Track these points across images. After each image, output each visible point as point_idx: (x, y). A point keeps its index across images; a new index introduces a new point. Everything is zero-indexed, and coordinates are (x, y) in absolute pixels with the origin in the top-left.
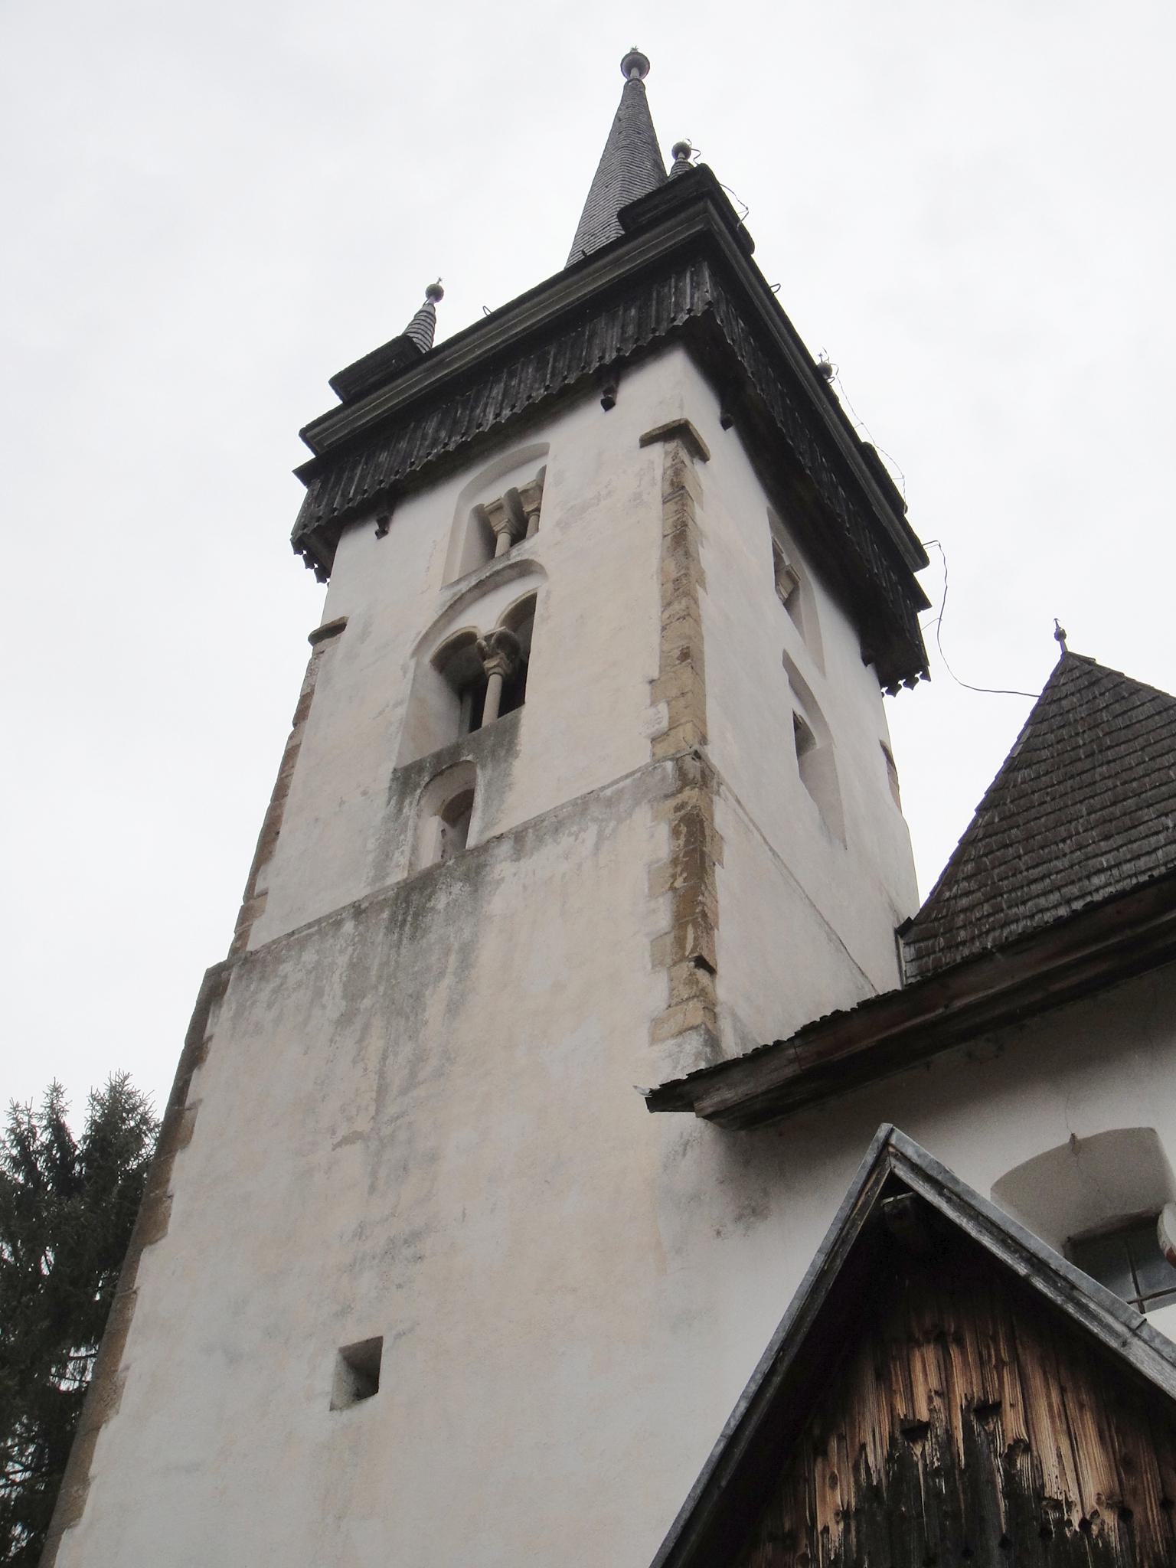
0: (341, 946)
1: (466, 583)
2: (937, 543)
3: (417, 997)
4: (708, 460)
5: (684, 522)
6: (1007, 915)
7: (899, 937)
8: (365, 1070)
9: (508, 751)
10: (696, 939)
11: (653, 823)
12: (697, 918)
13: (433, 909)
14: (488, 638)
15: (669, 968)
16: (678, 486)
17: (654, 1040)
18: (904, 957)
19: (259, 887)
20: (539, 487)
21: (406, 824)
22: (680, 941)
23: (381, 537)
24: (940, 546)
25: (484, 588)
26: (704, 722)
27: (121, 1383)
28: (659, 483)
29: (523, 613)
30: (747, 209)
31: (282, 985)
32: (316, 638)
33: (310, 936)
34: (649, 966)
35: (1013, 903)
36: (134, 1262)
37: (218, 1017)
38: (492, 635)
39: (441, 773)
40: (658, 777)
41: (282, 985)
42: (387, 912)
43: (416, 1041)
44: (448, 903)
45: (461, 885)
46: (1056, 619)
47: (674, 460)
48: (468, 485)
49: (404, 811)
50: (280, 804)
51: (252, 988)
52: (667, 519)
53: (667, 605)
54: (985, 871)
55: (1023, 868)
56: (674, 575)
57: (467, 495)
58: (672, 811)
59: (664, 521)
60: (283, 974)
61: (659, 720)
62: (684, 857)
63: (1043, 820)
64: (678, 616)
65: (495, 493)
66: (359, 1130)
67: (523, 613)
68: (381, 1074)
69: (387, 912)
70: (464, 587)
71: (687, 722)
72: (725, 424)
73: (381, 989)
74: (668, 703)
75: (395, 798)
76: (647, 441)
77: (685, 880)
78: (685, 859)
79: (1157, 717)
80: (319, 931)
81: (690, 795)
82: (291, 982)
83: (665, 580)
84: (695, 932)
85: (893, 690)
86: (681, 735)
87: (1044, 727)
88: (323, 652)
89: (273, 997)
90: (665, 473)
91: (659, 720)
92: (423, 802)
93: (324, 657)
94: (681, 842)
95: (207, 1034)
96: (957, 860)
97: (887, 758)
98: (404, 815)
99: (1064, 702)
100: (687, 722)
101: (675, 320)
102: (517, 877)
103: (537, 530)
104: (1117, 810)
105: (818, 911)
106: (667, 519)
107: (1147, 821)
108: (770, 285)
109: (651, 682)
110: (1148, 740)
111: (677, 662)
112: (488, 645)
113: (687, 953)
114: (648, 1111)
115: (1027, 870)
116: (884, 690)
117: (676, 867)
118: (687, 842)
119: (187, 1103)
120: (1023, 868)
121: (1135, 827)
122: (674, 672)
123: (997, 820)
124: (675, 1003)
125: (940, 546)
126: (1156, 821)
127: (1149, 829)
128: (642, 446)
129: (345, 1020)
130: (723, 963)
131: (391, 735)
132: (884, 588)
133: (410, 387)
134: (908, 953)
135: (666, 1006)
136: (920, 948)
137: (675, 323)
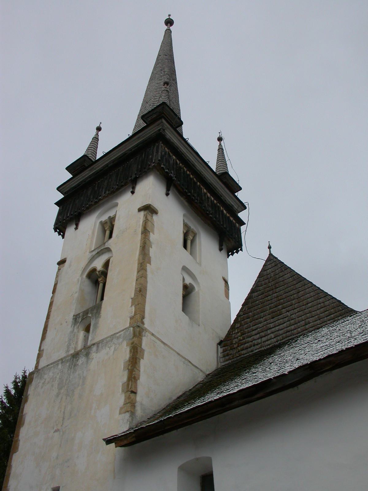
2: (247, 203)
4: (158, 213)
5: (145, 242)
6: (246, 340)
8: (61, 411)
10: (131, 385)
13: (78, 364)
14: (99, 272)
15: (126, 393)
17: (120, 413)
19: (42, 348)
20: (115, 215)
21: (74, 335)
22: (128, 385)
25: (99, 254)
26: (144, 312)
28: (141, 227)
29: (107, 264)
31: (45, 381)
33: (51, 367)
34: (121, 392)
38: (100, 271)
39: (84, 319)
40: (129, 333)
41: (45, 381)
48: (97, 216)
51: (38, 381)
53: (138, 272)
57: (98, 217)
59: (141, 241)
65: (105, 218)
66: (59, 428)
67: (107, 264)
68: (64, 413)
70: (94, 253)
71: (138, 314)
73: (66, 387)
74: (135, 306)
76: (140, 210)
77: (131, 367)
79: (290, 278)
81: (135, 340)
82: (47, 381)
84: (131, 383)
86: (137, 318)
87: (262, 279)
90: (143, 223)
92: (79, 327)
94: (131, 355)
95: (28, 394)
98: (75, 332)
100: (138, 314)
109: (132, 298)
110: (250, 325)
112: (99, 274)
115: (252, 326)
118: (133, 355)
120: (251, 326)
121: (280, 315)
123: (247, 309)
126: (286, 313)
129: (58, 395)
133: (86, 175)
134: (220, 350)
136: (224, 349)
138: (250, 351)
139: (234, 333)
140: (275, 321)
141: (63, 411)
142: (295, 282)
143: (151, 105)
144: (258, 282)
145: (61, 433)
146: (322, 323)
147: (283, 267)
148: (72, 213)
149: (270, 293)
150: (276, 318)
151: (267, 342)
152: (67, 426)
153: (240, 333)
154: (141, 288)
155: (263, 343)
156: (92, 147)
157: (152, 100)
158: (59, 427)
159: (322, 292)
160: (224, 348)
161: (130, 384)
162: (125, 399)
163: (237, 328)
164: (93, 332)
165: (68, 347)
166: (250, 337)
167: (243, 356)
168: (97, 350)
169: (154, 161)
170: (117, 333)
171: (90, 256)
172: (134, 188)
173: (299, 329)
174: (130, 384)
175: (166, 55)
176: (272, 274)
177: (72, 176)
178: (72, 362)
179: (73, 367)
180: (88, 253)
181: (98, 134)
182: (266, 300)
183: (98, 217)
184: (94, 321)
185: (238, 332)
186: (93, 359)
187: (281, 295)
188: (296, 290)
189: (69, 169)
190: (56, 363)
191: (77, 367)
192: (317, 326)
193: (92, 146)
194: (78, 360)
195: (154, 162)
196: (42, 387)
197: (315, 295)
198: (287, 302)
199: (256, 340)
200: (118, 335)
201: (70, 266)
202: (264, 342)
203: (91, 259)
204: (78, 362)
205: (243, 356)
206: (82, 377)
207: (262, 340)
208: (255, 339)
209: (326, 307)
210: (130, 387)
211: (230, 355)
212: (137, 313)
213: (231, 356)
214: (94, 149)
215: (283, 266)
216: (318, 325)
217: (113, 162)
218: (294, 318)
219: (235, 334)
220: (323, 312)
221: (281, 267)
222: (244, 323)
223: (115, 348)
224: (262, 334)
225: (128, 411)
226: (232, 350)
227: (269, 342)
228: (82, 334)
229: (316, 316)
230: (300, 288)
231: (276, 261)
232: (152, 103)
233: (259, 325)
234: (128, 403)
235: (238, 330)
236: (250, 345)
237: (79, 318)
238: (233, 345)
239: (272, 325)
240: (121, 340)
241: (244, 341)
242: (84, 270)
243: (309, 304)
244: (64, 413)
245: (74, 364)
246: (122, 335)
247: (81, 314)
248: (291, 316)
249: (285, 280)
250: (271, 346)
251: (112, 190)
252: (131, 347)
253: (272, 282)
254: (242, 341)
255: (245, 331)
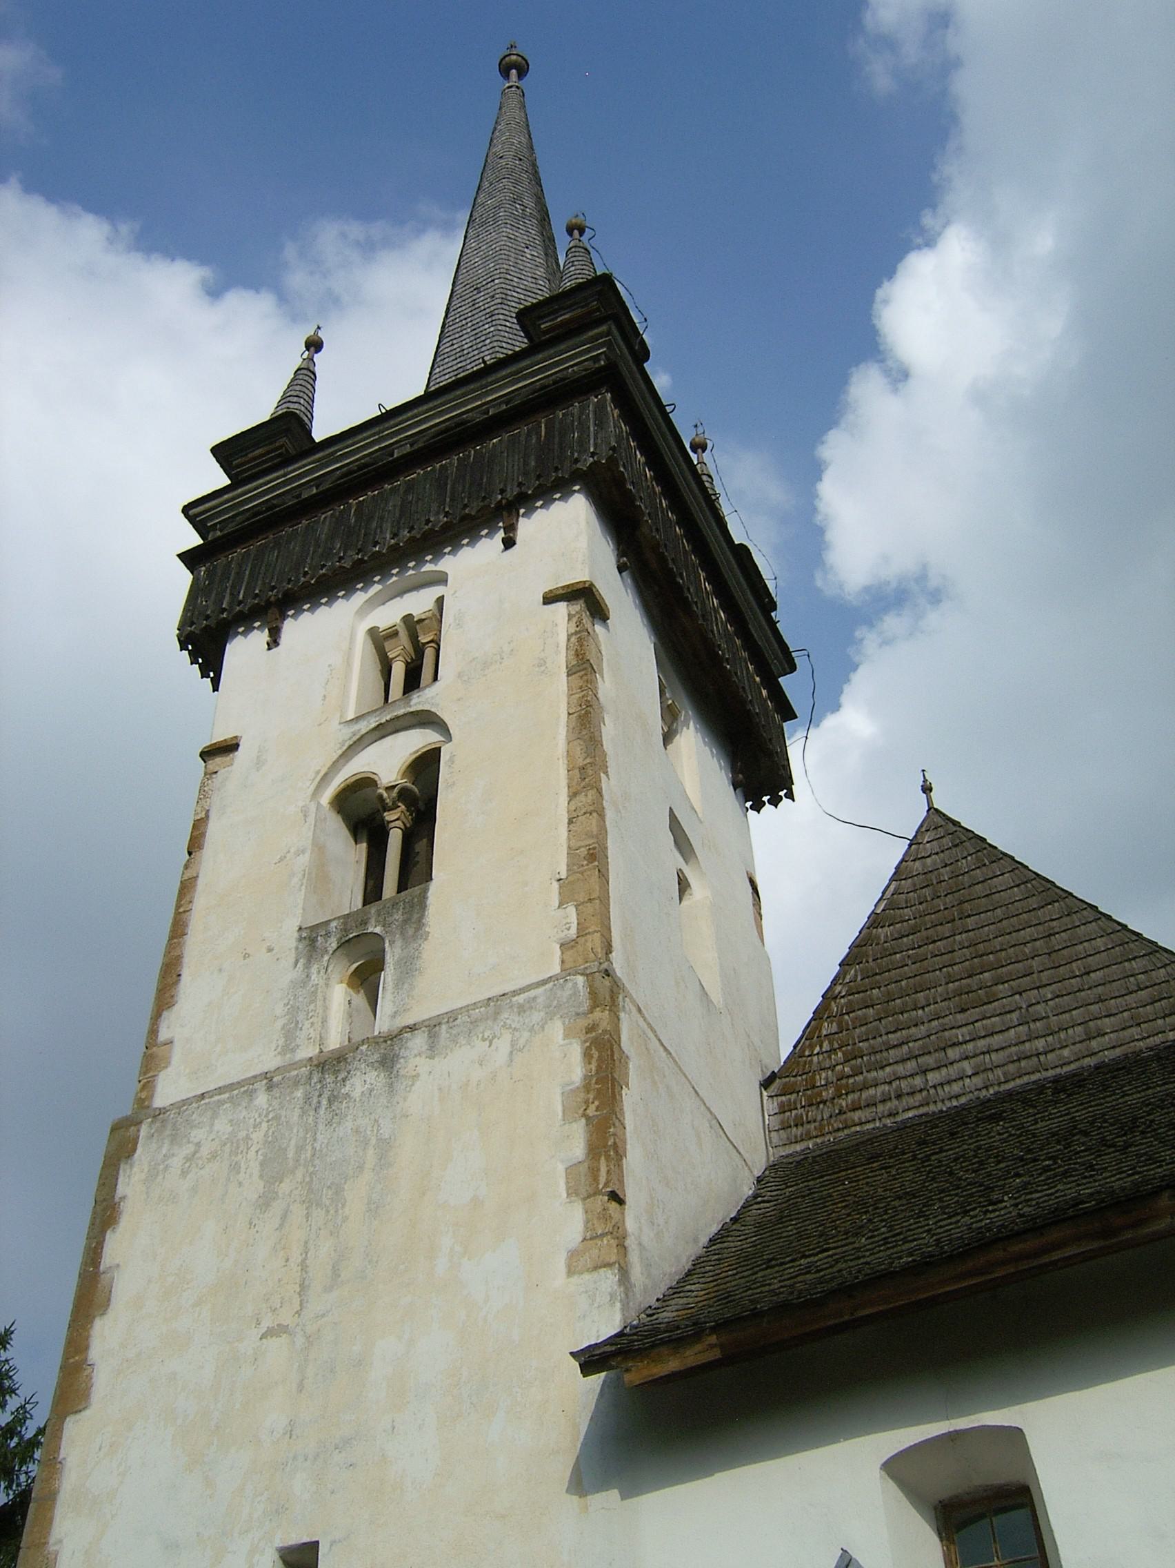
0: (255, 1120)
1: (365, 723)
3: (338, 1190)
6: (865, 1078)
7: (763, 1089)
9: (418, 929)
11: (566, 1041)
12: (609, 1151)
14: (390, 789)
16: (583, 658)
17: (570, 1272)
18: (768, 1110)
21: (314, 993)
22: (594, 1173)
23: (626, 1499)
24: (809, 656)
25: (382, 731)
27: (53, 1557)
30: (646, 320)
31: (195, 1152)
32: (208, 754)
33: (222, 1103)
35: (873, 1068)
36: (57, 1430)
37: (129, 1176)
38: (394, 787)
41: (195, 1152)
42: (301, 1091)
43: (338, 1237)
44: (363, 1092)
45: (376, 1074)
46: (923, 771)
47: (577, 626)
49: (313, 978)
50: (179, 943)
51: (164, 1151)
52: (572, 695)
53: (573, 796)
54: (847, 1030)
55: (883, 1032)
56: (580, 762)
58: (584, 1031)
59: (570, 695)
60: (196, 1140)
61: (568, 926)
62: (596, 1083)
63: (903, 983)
64: (584, 811)
65: (389, 615)
68: (304, 1266)
69: (301, 1091)
70: (365, 726)
71: (595, 931)
72: (621, 569)
74: (577, 907)
75: (301, 960)
76: (549, 599)
78: (597, 1086)
79: (1016, 889)
80: (231, 1099)
81: (602, 1016)
82: (205, 1151)
83: (571, 766)
85: (757, 807)
88: (216, 772)
89: (187, 1165)
91: (568, 926)
93: (218, 779)
94: (593, 1066)
96: (820, 1014)
97: (753, 889)
98: (312, 983)
99: (929, 860)
100: (595, 931)
101: (579, 461)
102: (431, 1077)
103: (435, 679)
104: (973, 982)
105: (702, 1100)
106: (572, 695)
107: (1002, 998)
108: (665, 403)
110: (877, 1029)
111: (585, 862)
113: (601, 1187)
114: (581, 1376)
116: (748, 804)
117: (588, 1093)
118: (599, 1068)
119: (102, 1268)
120: (883, 1032)
121: (990, 1003)
122: (582, 873)
123: (859, 978)
124: (591, 1237)
125: (809, 656)
126: (1009, 999)
127: (1004, 1007)
128: (545, 603)
129: (265, 1202)
130: (632, 1194)
131: (294, 887)
132: (757, 714)
134: (771, 1106)
135: (581, 1239)
137: (579, 466)
138: (886, 1113)
139: (817, 1050)
140: (971, 1020)
141: (296, 1257)
142: (1033, 902)
143: (497, 296)
144: (893, 895)
145: (300, 1341)
146: (1149, 1037)
147: (985, 852)
148: (257, 591)
149: (946, 929)
150: (972, 1010)
151: (947, 1088)
152: (323, 1316)
153: (840, 1054)
154: (594, 848)
155: (932, 1091)
156: (301, 394)
157: (497, 281)
158: (286, 1317)
159: (1136, 940)
160: (783, 1098)
161: (603, 1169)
162: (587, 1222)
163: (825, 1036)
164: (398, 984)
165: (290, 1034)
166: (882, 1068)
167: (858, 1128)
168: (432, 1047)
169: (595, 449)
170: (515, 993)
171: (346, 737)
172: (511, 529)
173: (1066, 1052)
174: (603, 1169)
175: (521, 160)
176: (945, 873)
177: (229, 482)
178: (319, 1086)
179: (324, 1102)
180: (335, 724)
181: (312, 360)
182: (932, 953)
183: (363, 611)
184: (398, 951)
185: (833, 1050)
186: (416, 1077)
187: (986, 938)
188: (1040, 927)
189: (225, 453)
190: (241, 1089)
191: (344, 1105)
192: (1132, 1044)
193: (300, 391)
194: (344, 1080)
195: (593, 454)
196: (184, 1173)
197: (1113, 948)
198: (1012, 963)
199: (905, 1077)
200: (520, 999)
201: (259, 763)
202: (934, 1087)
203: (350, 746)
204: (347, 1088)
205: (858, 1128)
206: (373, 1141)
207: (927, 1080)
208: (899, 1075)
209: (1156, 987)
210: (602, 1180)
211: (809, 1122)
212: (590, 930)
213: (812, 1126)
214: (306, 404)
215: (985, 848)
216: (1136, 1043)
217: (507, 403)
218: (1044, 1015)
219: (821, 1057)
220: (1150, 1001)
221: (979, 851)
222: (853, 1022)
223: (513, 1043)
224: (929, 1060)
225: (608, 1265)
226: (814, 1108)
227: (956, 1088)
228: (339, 995)
229: (1125, 1014)
230: (1055, 923)
231: (956, 831)
232: (498, 291)
233: (913, 1030)
234: (603, 1235)
235: (831, 1043)
236: (883, 1093)
237: (328, 935)
238: (816, 1090)
239: (961, 1034)
240: (537, 1017)
241: (859, 1078)
242: (325, 778)
243: (1092, 975)
244: (304, 1266)
245: (326, 1094)
246: (539, 1000)
247: (334, 924)
248: (1029, 1009)
249: (997, 895)
250: (963, 1100)
251: (427, 527)
252: (585, 1042)
253: (946, 896)
254: (851, 1081)
255: (860, 1049)
